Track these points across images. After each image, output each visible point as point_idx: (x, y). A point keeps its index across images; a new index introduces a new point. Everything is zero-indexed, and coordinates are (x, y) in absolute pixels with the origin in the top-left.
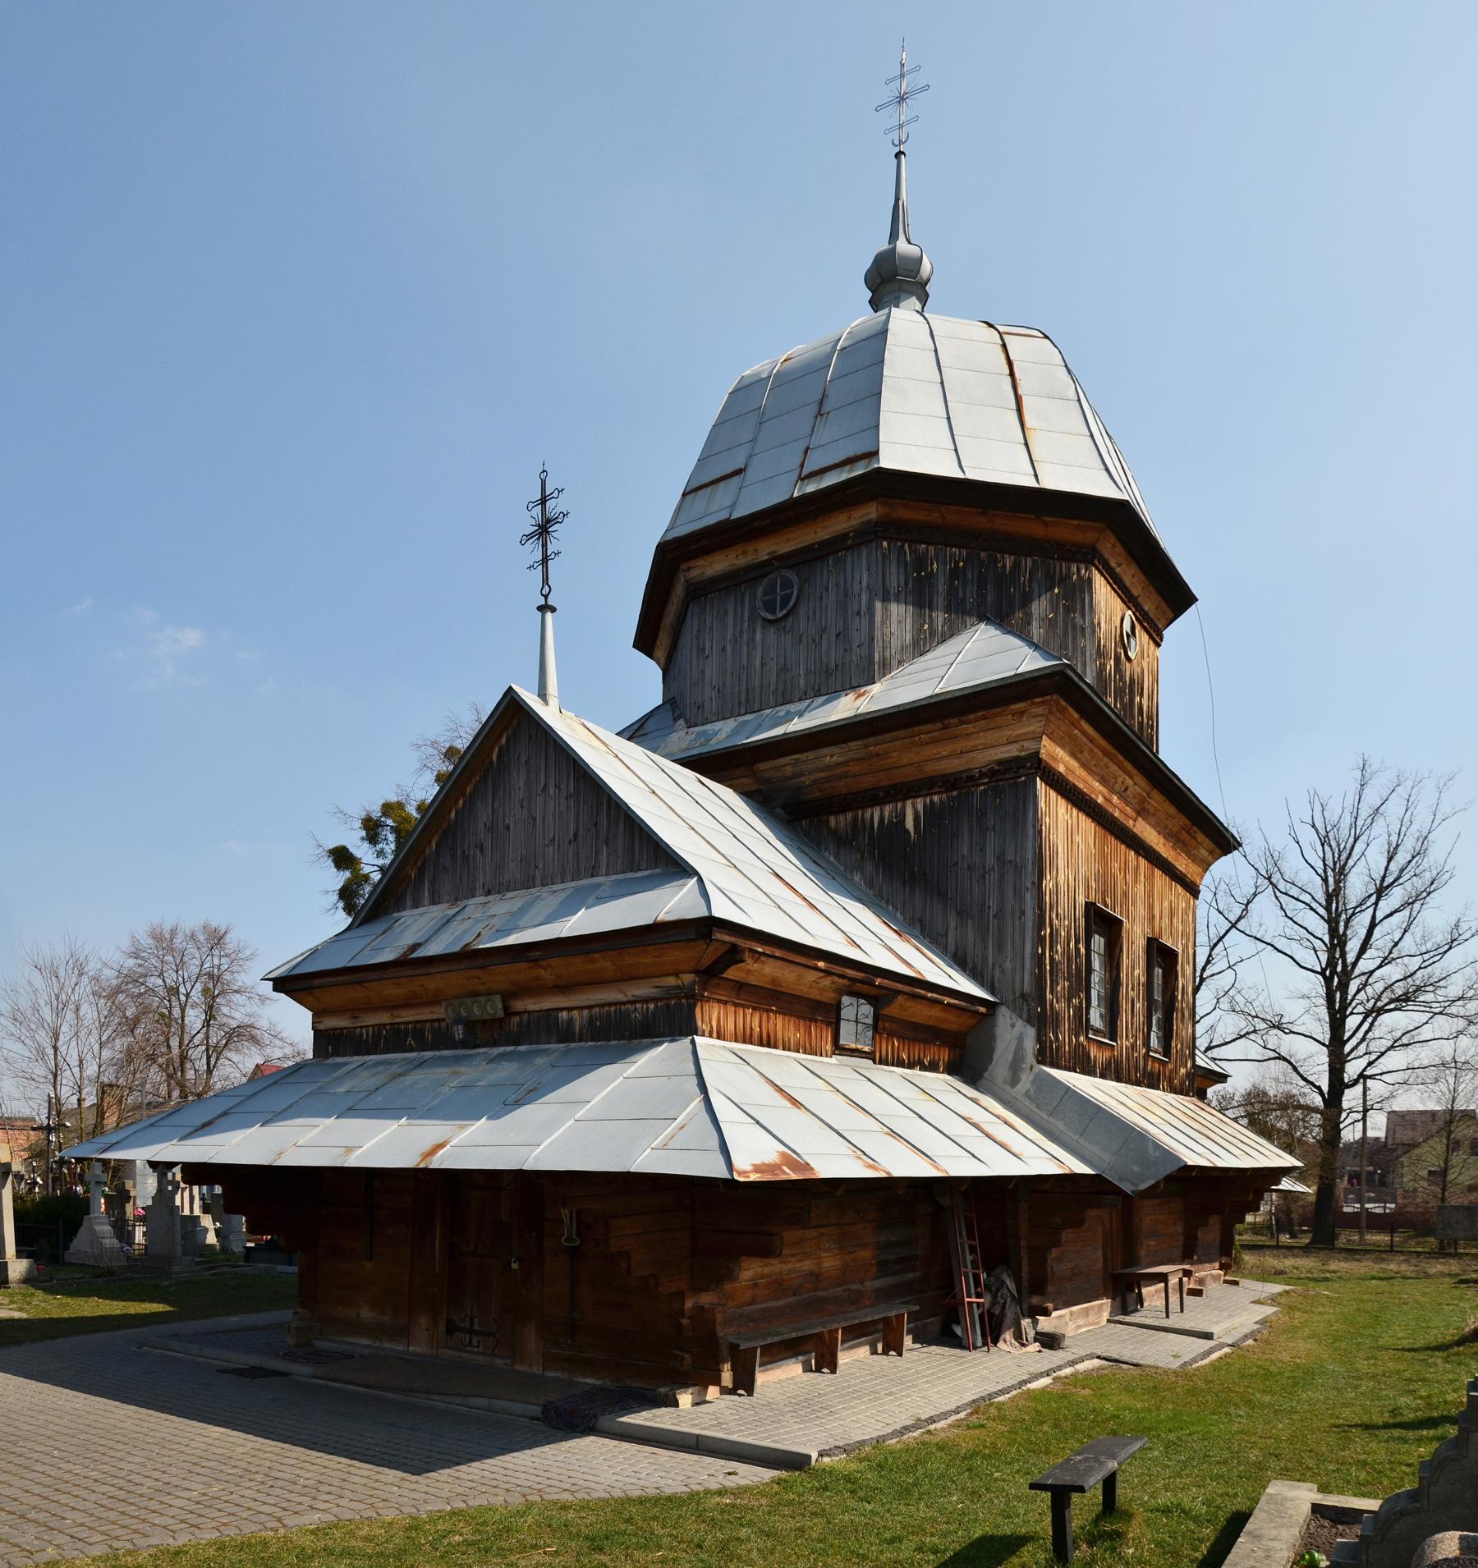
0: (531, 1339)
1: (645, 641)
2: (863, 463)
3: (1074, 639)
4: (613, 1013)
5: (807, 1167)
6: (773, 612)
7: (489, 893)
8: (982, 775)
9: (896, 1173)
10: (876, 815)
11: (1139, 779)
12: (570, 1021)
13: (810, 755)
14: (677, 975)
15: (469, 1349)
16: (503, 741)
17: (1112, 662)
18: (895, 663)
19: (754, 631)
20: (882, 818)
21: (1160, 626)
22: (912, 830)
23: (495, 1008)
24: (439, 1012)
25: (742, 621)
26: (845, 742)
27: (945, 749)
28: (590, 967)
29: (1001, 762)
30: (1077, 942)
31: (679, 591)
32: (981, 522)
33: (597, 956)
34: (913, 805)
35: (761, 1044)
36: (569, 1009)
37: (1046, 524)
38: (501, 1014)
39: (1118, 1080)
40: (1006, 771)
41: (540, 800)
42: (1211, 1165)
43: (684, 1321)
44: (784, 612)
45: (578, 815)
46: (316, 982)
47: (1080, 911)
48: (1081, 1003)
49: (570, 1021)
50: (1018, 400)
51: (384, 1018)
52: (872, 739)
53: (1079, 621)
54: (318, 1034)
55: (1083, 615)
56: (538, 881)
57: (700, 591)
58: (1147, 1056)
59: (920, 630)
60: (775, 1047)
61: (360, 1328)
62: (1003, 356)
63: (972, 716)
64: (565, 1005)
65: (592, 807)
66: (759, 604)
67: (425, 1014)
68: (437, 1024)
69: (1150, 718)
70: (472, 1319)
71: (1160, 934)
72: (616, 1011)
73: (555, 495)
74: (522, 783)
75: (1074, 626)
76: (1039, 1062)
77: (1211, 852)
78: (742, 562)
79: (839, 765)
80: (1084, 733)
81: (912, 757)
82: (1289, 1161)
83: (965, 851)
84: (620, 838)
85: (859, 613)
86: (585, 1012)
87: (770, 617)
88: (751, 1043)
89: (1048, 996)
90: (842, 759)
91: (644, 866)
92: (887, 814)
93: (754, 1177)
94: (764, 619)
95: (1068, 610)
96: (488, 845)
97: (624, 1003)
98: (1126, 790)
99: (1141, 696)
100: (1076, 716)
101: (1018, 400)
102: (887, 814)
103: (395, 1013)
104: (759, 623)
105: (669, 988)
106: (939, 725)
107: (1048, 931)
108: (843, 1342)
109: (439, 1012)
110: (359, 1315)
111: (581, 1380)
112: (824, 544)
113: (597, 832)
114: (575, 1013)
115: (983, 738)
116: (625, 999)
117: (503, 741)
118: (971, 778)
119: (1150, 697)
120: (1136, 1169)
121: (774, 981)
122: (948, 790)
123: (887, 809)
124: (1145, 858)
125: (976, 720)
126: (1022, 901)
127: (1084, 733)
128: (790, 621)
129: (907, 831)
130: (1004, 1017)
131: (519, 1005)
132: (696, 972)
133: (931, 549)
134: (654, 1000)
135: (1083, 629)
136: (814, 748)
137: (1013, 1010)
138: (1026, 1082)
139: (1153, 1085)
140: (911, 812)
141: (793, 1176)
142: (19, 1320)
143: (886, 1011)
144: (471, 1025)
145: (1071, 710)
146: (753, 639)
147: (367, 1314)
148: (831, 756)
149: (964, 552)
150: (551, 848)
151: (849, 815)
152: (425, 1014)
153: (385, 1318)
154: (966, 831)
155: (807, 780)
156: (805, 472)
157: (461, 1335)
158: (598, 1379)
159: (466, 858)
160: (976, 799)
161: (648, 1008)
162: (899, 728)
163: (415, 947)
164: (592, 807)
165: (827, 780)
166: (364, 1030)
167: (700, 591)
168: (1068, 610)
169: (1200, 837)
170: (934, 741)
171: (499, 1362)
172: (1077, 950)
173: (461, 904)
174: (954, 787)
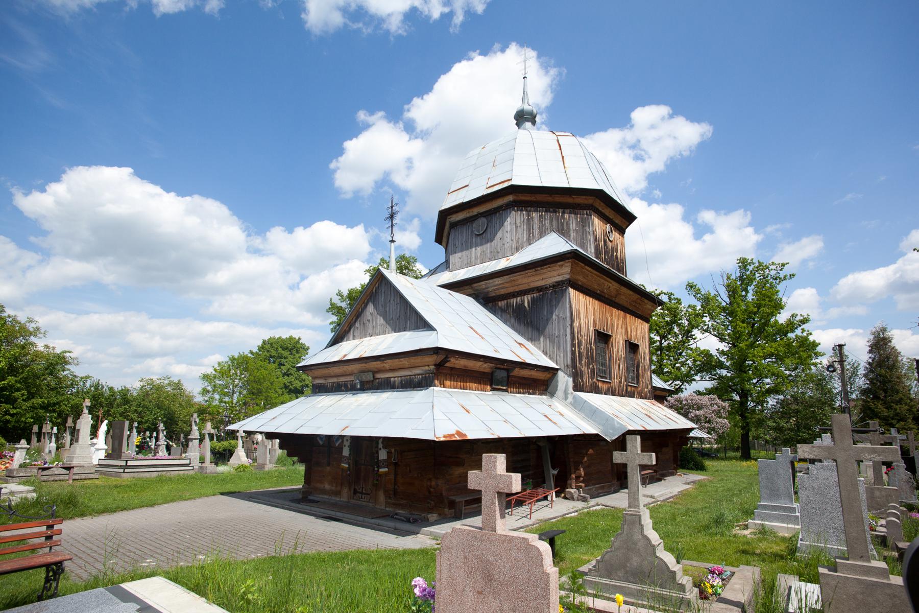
0: (382, 497)
1: (439, 240)
2: (507, 182)
3: (586, 236)
5: (465, 435)
7: (371, 336)
9: (470, 436)
10: (514, 301)
11: (614, 283)
12: (395, 381)
13: (491, 281)
14: (428, 366)
16: (377, 285)
17: (603, 243)
20: (516, 302)
21: (624, 227)
22: (527, 306)
23: (369, 377)
24: (352, 378)
26: (503, 276)
27: (536, 278)
28: (401, 363)
29: (556, 282)
30: (591, 344)
32: (550, 199)
34: (527, 298)
36: (394, 377)
37: (573, 198)
38: (372, 379)
39: (613, 395)
40: (558, 285)
41: (388, 305)
42: (643, 429)
43: (432, 490)
46: (313, 368)
47: (592, 334)
48: (593, 367)
49: (395, 381)
50: (563, 157)
51: (335, 380)
52: (512, 275)
53: (588, 230)
55: (589, 227)
56: (387, 332)
57: (454, 225)
58: (627, 385)
59: (529, 236)
61: (324, 492)
62: (557, 143)
63: (545, 267)
67: (348, 378)
69: (621, 260)
70: (362, 488)
71: (631, 338)
75: (586, 232)
76: (575, 391)
77: (652, 306)
78: (468, 215)
79: (501, 284)
80: (588, 270)
81: (525, 281)
82: (694, 426)
83: (545, 313)
86: (400, 378)
89: (578, 365)
92: (518, 301)
93: (442, 439)
94: (476, 235)
95: (583, 226)
96: (371, 320)
98: (609, 287)
99: (617, 252)
100: (583, 265)
101: (563, 157)
102: (518, 301)
105: (426, 371)
106: (534, 270)
107: (577, 341)
109: (352, 378)
112: (495, 209)
115: (552, 273)
117: (377, 285)
118: (546, 288)
119: (622, 252)
120: (611, 431)
121: (465, 366)
122: (539, 292)
123: (518, 299)
124: (622, 310)
125: (546, 268)
126: (566, 331)
127: (588, 270)
128: (484, 235)
129: (525, 307)
131: (378, 376)
132: (435, 365)
134: (422, 374)
135: (589, 233)
136: (492, 278)
137: (564, 372)
138: (570, 399)
140: (526, 300)
141: (458, 438)
142: (426, 527)
143: (511, 374)
145: (580, 263)
147: (327, 487)
148: (498, 281)
151: (506, 301)
152: (348, 378)
154: (545, 306)
155: (490, 289)
156: (488, 186)
159: (364, 324)
163: (345, 356)
165: (497, 289)
167: (454, 225)
168: (583, 226)
169: (646, 301)
171: (371, 504)
172: (591, 348)
173: (362, 340)
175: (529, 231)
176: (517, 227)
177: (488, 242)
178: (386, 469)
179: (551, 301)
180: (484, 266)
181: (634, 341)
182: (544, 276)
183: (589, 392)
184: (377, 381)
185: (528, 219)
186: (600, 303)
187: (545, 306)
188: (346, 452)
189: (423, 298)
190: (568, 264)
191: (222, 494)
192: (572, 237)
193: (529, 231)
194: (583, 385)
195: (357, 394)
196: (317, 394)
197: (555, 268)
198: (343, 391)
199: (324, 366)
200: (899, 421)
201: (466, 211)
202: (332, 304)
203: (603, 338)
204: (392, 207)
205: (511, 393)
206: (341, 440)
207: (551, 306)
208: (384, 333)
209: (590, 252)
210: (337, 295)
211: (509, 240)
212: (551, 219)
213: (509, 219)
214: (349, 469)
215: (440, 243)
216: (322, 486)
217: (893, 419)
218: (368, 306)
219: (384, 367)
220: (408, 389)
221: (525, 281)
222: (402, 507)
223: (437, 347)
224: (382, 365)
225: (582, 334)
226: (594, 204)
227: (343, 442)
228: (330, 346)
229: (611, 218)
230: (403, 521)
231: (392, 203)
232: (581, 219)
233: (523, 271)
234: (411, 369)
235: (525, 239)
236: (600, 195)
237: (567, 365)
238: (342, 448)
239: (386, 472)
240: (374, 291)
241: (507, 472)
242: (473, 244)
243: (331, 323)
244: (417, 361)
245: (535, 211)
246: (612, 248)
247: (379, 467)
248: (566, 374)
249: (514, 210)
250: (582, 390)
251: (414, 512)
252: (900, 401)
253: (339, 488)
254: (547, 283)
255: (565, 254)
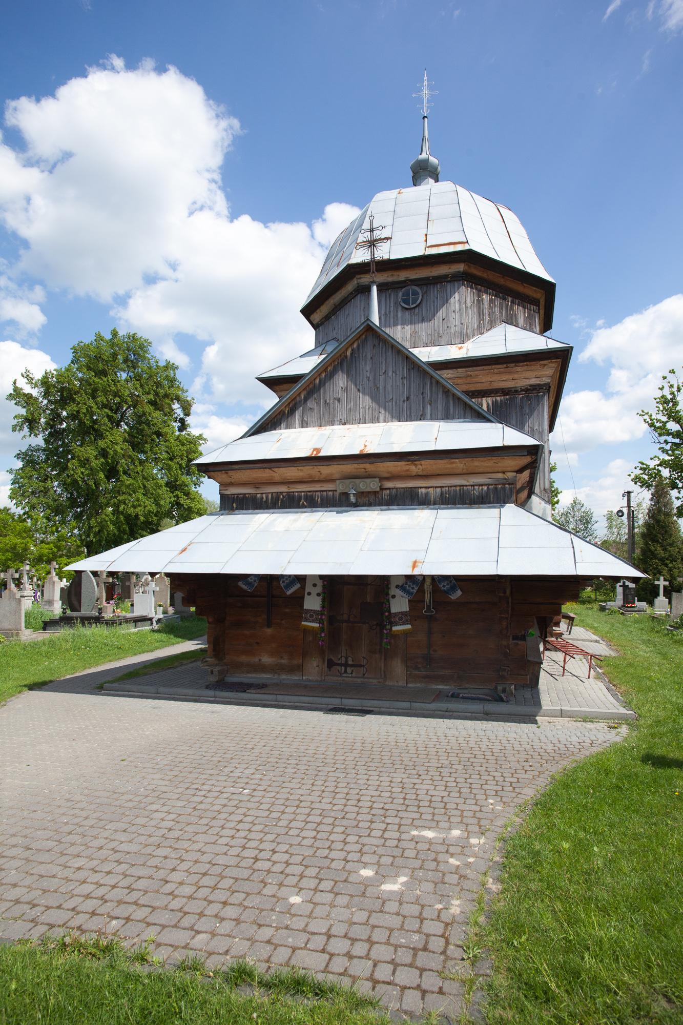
0: (398, 667)
2: (452, 246)
4: (458, 492)
6: (408, 304)
8: (522, 390)
12: (427, 494)
14: (504, 473)
15: (345, 675)
16: (355, 346)
18: (471, 336)
19: (397, 312)
23: (373, 485)
25: (390, 307)
29: (531, 386)
32: (501, 281)
33: (457, 460)
36: (426, 488)
40: (534, 389)
44: (414, 305)
45: (410, 388)
46: (230, 467)
51: (283, 489)
54: (223, 497)
61: (262, 668)
63: (522, 364)
64: (425, 485)
65: (419, 384)
66: (400, 300)
68: (325, 493)
70: (346, 658)
72: (460, 490)
73: (380, 228)
74: (368, 368)
78: (390, 279)
84: (439, 402)
85: (454, 311)
86: (439, 490)
87: (407, 306)
90: (452, 376)
91: (457, 417)
94: (403, 307)
97: (466, 486)
103: (291, 486)
104: (400, 308)
106: (505, 365)
110: (260, 660)
111: (434, 687)
113: (423, 398)
114: (431, 490)
116: (468, 484)
117: (355, 346)
118: (516, 391)
125: (522, 366)
128: (417, 310)
134: (488, 485)
137: (540, 497)
139: (153, 528)
144: (360, 494)
146: (397, 316)
147: (267, 659)
150: (390, 404)
153: (283, 661)
154: (514, 414)
157: (339, 668)
158: (446, 685)
160: (518, 400)
161: (482, 489)
164: (419, 384)
166: (264, 495)
170: (500, 373)
174: (507, 394)
176: (467, 307)
177: (423, 320)
178: (409, 627)
179: (522, 408)
182: (516, 376)
185: (478, 300)
187: (514, 414)
188: (313, 603)
190: (553, 365)
191: (32, 687)
195: (347, 511)
196: (237, 512)
197: (533, 368)
198: (304, 507)
199: (266, 465)
200: (671, 561)
201: (390, 273)
202: (16, 389)
206: (298, 586)
207: (523, 415)
208: (375, 420)
210: (22, 375)
211: (457, 323)
212: (501, 308)
213: (457, 295)
214: (322, 629)
216: (256, 660)
217: (667, 559)
218: (336, 377)
219: (408, 470)
220: (250, 511)
221: (488, 379)
222: (443, 679)
224: (407, 467)
227: (303, 588)
230: (488, 700)
232: (529, 314)
233: (489, 365)
235: (476, 326)
237: (545, 489)
238: (303, 598)
239: (409, 629)
240: (349, 353)
242: (397, 320)
243: (16, 417)
244: (486, 464)
245: (485, 292)
247: (392, 624)
248: (544, 499)
249: (463, 284)
251: (467, 686)
252: (671, 545)
253: (297, 661)
254: (517, 385)
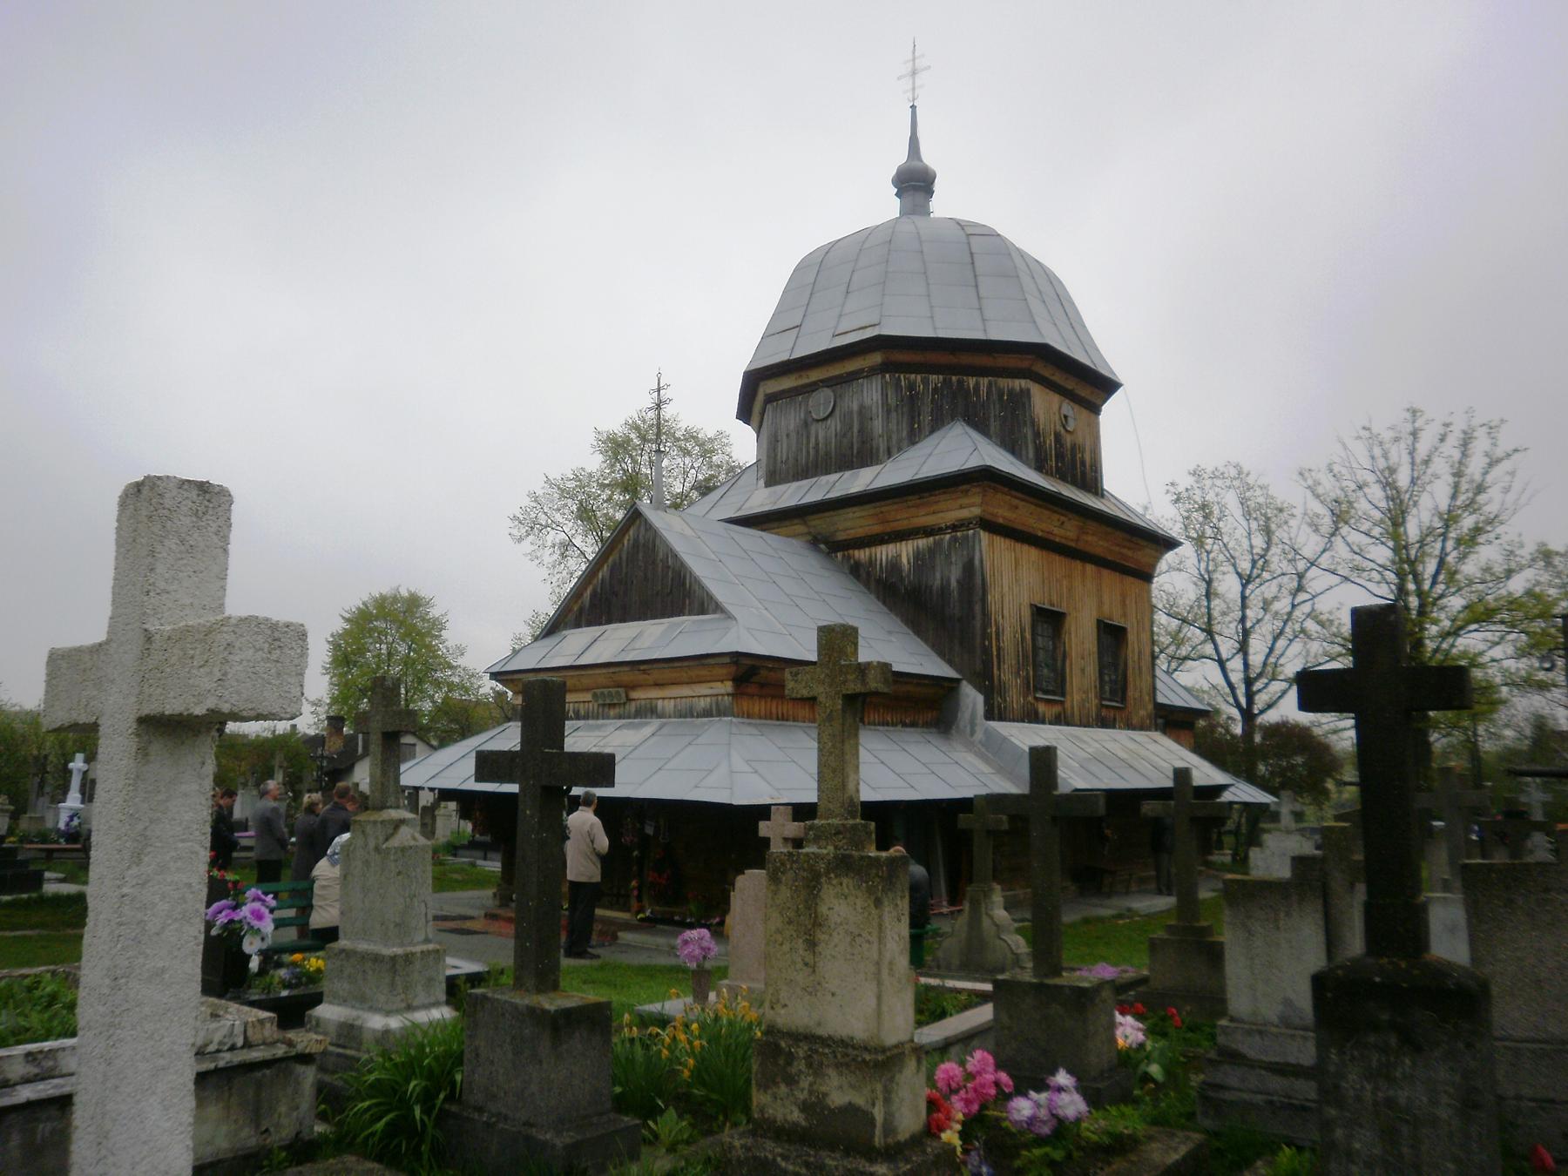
8: (947, 528)
17: (1052, 437)
31: (760, 397)
35: (778, 719)
39: (1068, 724)
40: (962, 525)
48: (1028, 674)
57: (771, 399)
60: (787, 720)
88: (771, 719)
108: (1247, 873)
130: (965, 684)
131: (634, 695)
133: (919, 377)
138: (979, 735)
149: (941, 377)
162: (894, 497)
175: (913, 418)
180: (828, 482)
181: (1118, 621)
182: (935, 507)
183: (1018, 721)
184: (633, 704)
186: (1045, 553)
189: (713, 557)
192: (992, 428)
193: (913, 418)
194: (1005, 707)
201: (793, 377)
203: (1049, 620)
204: (659, 391)
205: (869, 724)
209: (1027, 458)
215: (747, 422)
223: (737, 652)
225: (1006, 613)
226: (1033, 368)
228: (544, 637)
229: (1070, 387)
231: (659, 384)
234: (693, 686)
236: (1044, 352)
241: (477, 780)
246: (1074, 447)
250: (1001, 718)
255: (972, 472)
